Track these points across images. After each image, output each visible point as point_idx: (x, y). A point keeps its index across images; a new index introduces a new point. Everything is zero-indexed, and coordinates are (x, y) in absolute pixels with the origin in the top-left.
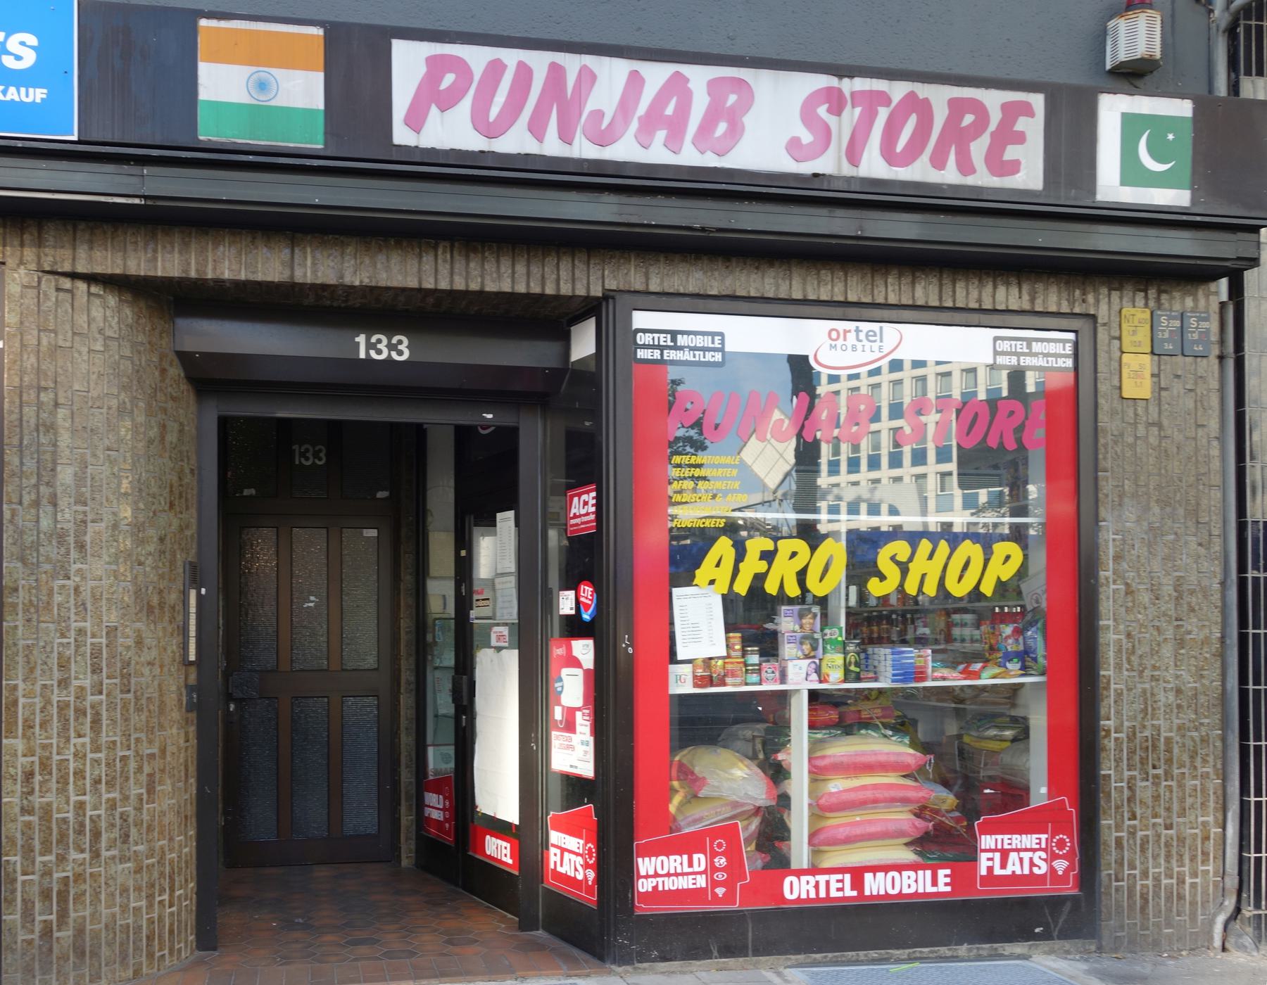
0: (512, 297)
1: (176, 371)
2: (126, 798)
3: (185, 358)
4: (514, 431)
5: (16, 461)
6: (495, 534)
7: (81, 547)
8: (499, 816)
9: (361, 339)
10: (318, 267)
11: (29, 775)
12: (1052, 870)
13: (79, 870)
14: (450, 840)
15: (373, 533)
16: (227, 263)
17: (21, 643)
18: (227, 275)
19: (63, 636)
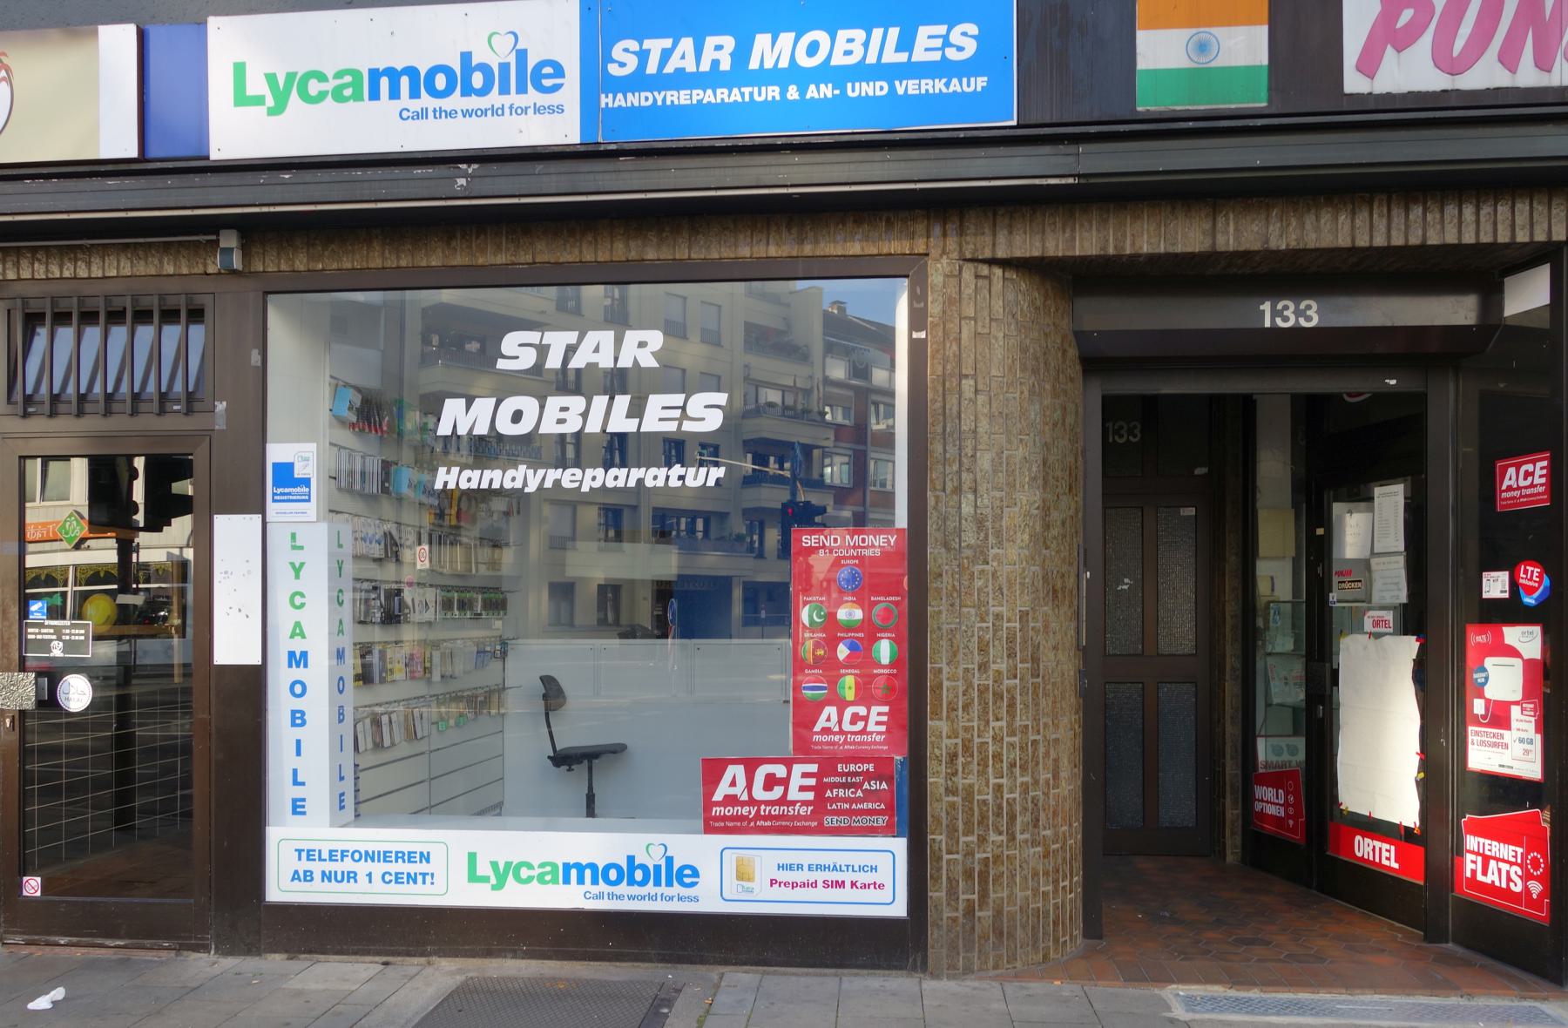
0: (1388, 251)
1: (1073, 352)
2: (1036, 782)
3: (1080, 336)
4: (1420, 399)
5: (940, 449)
6: (1371, 510)
7: (998, 534)
8: (1378, 815)
9: (1266, 307)
10: (1240, 233)
11: (953, 757)
12: (1527, 889)
13: (998, 852)
14: (1298, 837)
15: (1191, 511)
16: (1145, 237)
17: (945, 627)
18: (1145, 249)
19: (983, 620)
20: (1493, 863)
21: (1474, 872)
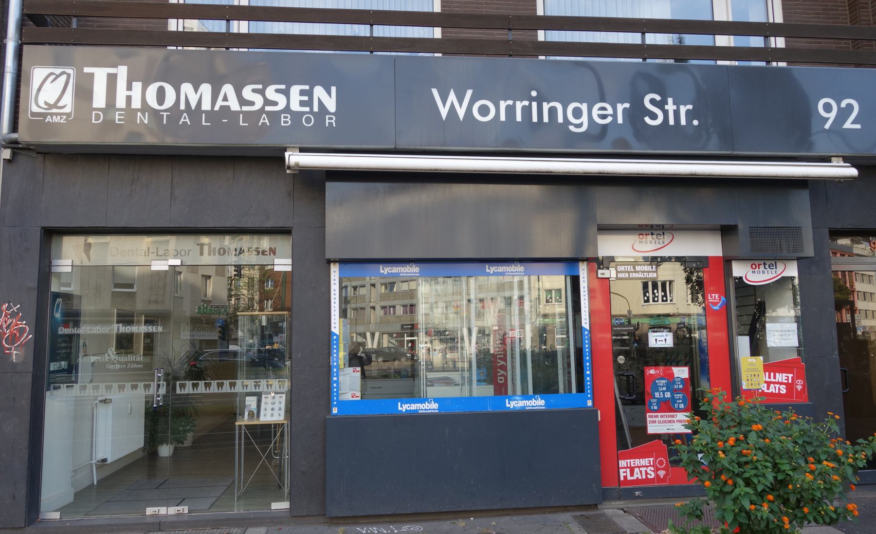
12: (657, 476)
20: (637, 470)
21: (625, 477)
